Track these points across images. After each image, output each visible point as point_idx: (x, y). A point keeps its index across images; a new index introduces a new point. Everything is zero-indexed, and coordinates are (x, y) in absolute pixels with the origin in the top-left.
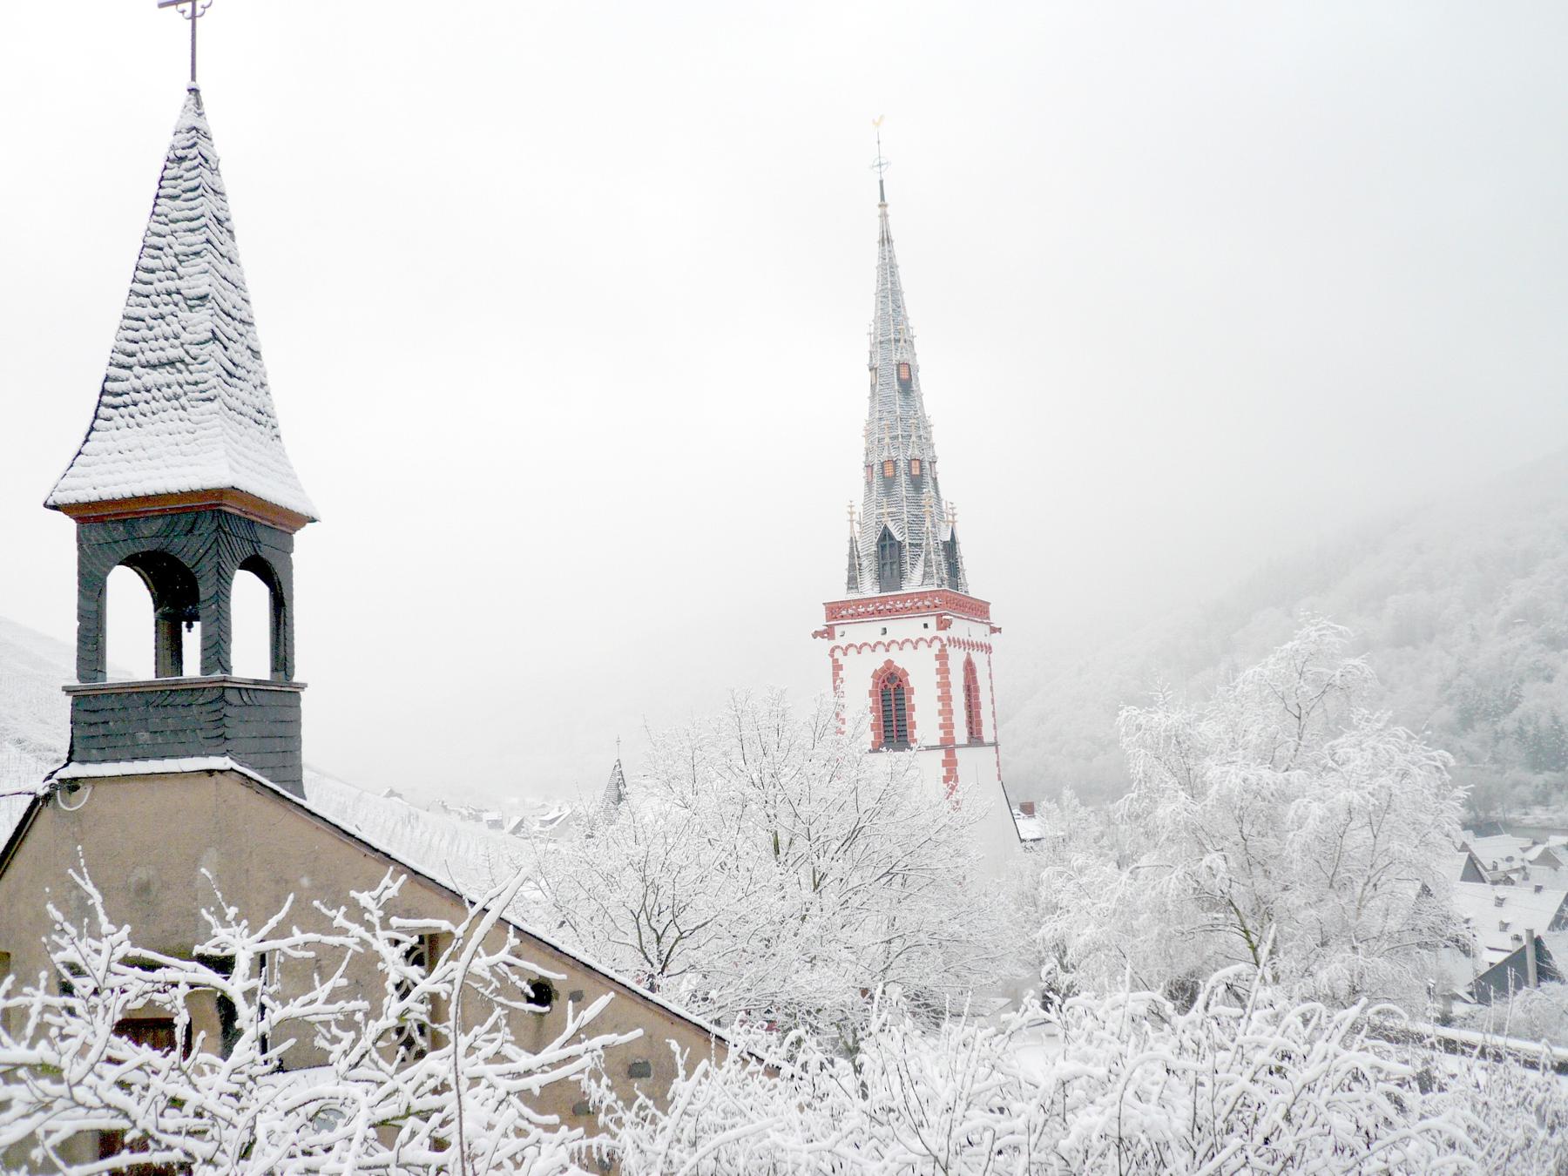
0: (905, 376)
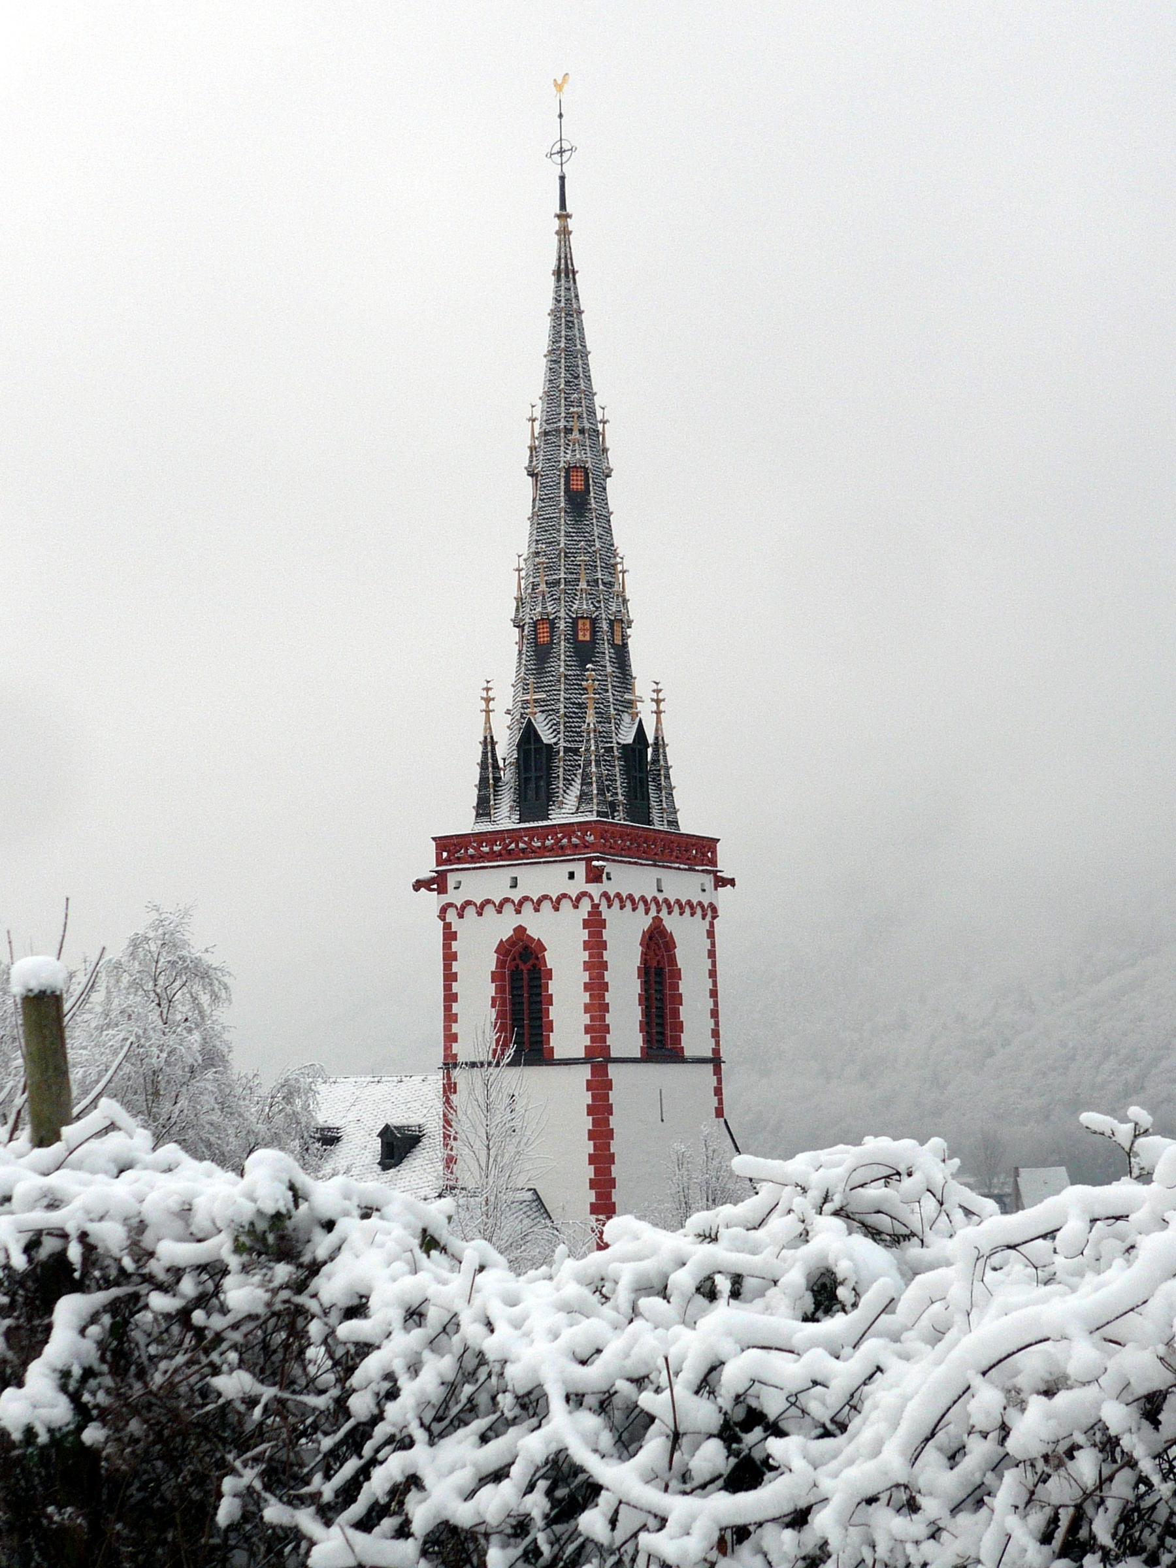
0: (577, 485)
